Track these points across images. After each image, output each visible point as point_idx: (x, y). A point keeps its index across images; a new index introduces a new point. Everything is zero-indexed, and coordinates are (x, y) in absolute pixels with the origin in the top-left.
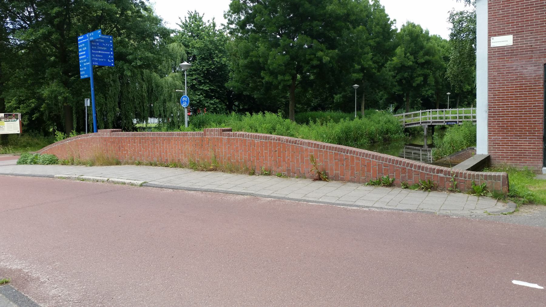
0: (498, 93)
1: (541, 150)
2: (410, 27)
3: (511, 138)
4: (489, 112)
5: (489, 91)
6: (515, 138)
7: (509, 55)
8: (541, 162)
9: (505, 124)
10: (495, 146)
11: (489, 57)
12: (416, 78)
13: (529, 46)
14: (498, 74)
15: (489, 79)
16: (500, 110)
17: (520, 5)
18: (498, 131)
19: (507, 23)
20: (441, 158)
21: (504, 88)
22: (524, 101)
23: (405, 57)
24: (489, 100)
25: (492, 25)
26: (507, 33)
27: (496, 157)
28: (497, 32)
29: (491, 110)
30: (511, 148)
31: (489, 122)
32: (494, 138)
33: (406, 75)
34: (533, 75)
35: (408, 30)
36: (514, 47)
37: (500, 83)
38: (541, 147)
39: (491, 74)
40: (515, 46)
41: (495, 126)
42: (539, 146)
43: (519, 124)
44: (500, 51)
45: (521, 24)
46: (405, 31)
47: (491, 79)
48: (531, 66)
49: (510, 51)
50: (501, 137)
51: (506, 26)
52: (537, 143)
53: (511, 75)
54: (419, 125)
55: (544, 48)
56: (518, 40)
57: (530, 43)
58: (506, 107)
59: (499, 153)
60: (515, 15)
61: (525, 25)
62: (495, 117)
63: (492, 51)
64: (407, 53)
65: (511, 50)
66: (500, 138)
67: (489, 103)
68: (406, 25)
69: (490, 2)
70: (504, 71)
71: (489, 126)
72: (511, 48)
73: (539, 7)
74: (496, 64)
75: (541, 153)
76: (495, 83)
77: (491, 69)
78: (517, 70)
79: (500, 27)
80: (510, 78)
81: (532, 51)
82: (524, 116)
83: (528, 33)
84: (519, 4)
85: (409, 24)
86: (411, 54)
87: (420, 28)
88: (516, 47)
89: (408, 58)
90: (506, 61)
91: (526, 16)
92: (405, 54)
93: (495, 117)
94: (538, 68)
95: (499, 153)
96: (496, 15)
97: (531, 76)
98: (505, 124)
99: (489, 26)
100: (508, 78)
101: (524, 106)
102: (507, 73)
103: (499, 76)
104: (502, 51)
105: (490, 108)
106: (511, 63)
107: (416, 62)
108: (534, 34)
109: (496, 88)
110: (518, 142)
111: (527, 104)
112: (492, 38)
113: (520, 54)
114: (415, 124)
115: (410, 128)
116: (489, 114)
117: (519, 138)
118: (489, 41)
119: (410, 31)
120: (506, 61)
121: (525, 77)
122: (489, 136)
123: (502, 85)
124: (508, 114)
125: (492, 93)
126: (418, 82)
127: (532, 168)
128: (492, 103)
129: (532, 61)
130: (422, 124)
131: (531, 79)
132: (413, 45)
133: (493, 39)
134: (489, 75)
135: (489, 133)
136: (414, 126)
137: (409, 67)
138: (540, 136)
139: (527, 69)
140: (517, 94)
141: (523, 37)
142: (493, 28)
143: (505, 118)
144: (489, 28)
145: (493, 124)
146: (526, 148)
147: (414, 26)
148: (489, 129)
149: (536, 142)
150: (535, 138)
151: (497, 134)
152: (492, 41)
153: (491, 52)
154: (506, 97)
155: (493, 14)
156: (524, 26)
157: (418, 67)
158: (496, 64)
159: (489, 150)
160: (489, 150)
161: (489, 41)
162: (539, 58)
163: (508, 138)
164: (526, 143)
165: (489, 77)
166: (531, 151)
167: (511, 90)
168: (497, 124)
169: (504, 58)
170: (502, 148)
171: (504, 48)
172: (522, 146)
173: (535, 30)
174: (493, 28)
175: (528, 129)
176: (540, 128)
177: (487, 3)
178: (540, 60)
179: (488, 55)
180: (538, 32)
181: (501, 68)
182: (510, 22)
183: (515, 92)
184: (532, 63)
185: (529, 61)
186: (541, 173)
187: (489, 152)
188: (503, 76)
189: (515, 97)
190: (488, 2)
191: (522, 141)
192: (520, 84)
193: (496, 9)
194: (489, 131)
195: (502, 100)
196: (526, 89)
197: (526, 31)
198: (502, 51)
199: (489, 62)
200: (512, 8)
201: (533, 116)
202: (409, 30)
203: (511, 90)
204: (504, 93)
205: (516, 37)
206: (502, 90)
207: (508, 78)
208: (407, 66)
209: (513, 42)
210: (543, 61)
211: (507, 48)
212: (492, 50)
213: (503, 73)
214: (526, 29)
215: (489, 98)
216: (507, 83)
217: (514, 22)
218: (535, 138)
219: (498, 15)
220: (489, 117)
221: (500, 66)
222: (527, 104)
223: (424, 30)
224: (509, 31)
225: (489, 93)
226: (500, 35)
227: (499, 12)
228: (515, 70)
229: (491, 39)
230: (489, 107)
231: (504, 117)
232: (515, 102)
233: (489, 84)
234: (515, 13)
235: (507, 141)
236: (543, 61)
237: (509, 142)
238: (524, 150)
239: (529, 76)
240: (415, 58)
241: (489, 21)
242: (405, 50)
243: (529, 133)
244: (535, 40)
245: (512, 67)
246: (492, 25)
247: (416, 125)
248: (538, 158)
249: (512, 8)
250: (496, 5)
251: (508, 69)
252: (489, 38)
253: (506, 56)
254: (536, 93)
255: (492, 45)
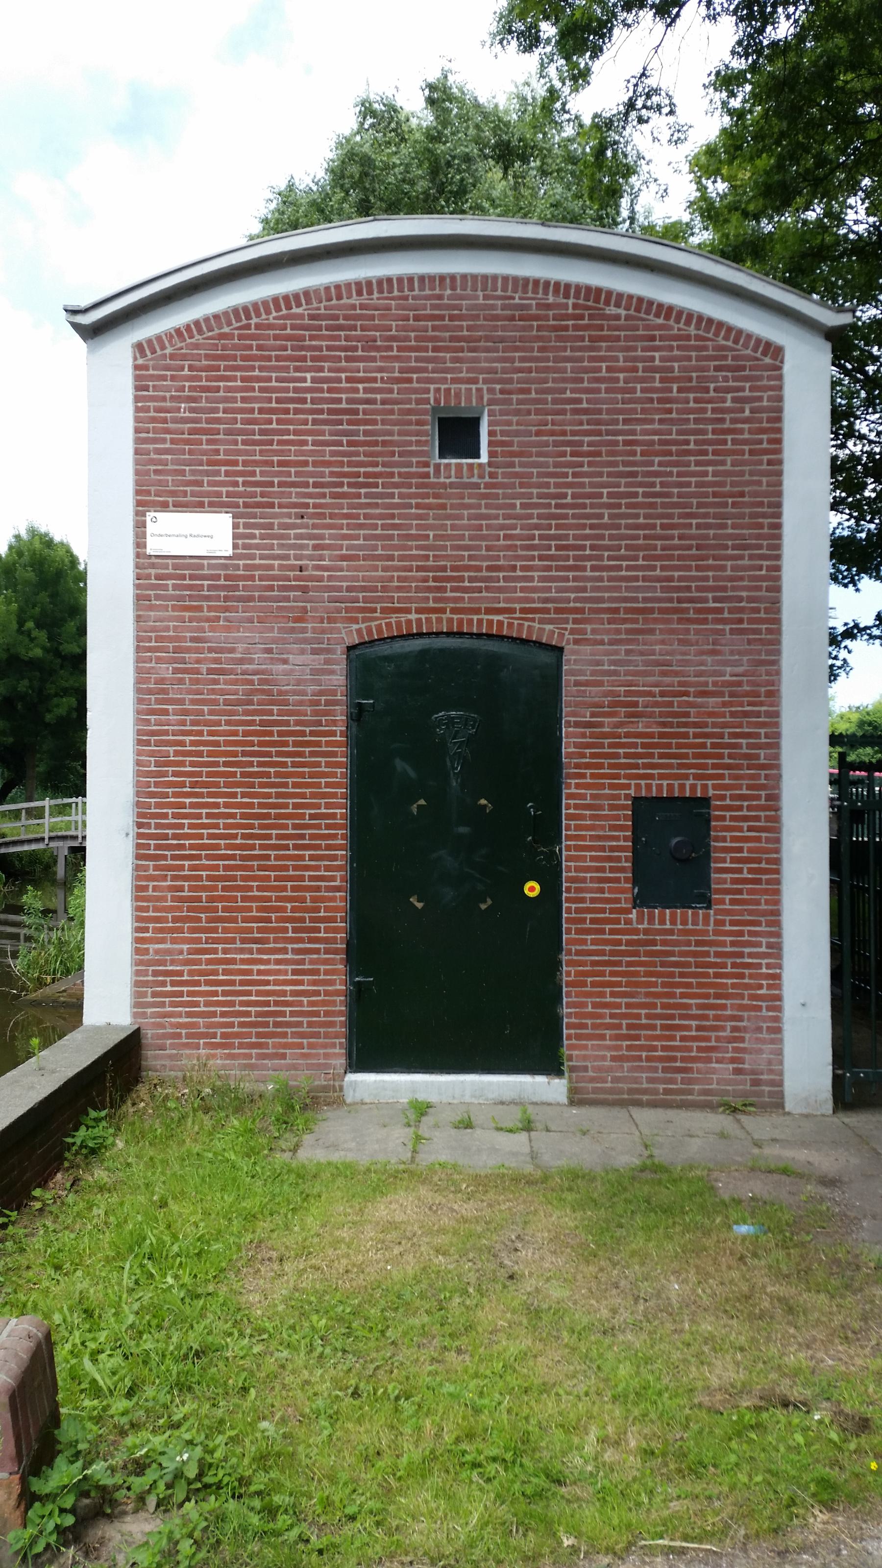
0: (177, 753)
1: (338, 999)
2: (37, 545)
3: (225, 951)
4: (139, 836)
5: (139, 742)
6: (242, 951)
7: (218, 598)
8: (337, 1051)
9: (204, 888)
10: (164, 983)
11: (138, 598)
12: (56, 700)
13: (291, 568)
14: (176, 671)
15: (138, 691)
16: (181, 826)
17: (257, 394)
18: (175, 920)
19: (210, 463)
20: (53, 980)
21: (201, 733)
22: (279, 795)
23: (20, 631)
24: (138, 784)
25: (152, 462)
26: (211, 505)
27: (165, 1036)
28: (173, 493)
29: (148, 826)
30: (225, 994)
31: (138, 878)
32: (157, 952)
33: (23, 685)
34: (311, 688)
35: (29, 550)
36: (237, 567)
37: (185, 712)
38: (338, 987)
39: (149, 671)
40: (241, 562)
41: (164, 899)
42: (332, 983)
43: (259, 889)
44: (183, 577)
45: (262, 473)
46: (20, 554)
47: (150, 692)
48: (303, 652)
49: (222, 582)
50: (185, 947)
51: (207, 473)
52: (326, 972)
53: (226, 682)
54: (41, 846)
55: (345, 584)
56: (253, 536)
57: (297, 558)
58: (208, 816)
59: (180, 1015)
60: (241, 432)
61: (276, 480)
62: (164, 857)
63: (153, 572)
64: (25, 621)
65: (227, 578)
66: (181, 952)
67: (138, 794)
68: (24, 534)
69: (140, 361)
70: (198, 661)
71: (137, 899)
72: (225, 567)
73: (325, 416)
74: (167, 629)
75: (340, 1013)
76: (166, 712)
77: (150, 649)
78: (251, 661)
79: (182, 473)
80: (223, 692)
81: (305, 590)
82: (277, 858)
83: (289, 516)
84: (253, 389)
85: (33, 532)
86: (39, 626)
87: (69, 551)
88: (247, 567)
89: (29, 635)
90: (208, 620)
91: (280, 443)
92: (21, 623)
93: (164, 857)
94: (327, 662)
95: (180, 1015)
96: (165, 421)
97: (303, 693)
98: (204, 888)
99: (137, 463)
100: (213, 692)
101: (278, 816)
102: (210, 671)
103: (181, 681)
104: (192, 577)
105: (142, 818)
106: (228, 629)
107: (57, 653)
108: (311, 522)
109: (166, 733)
110: (255, 968)
111: (286, 806)
112: (152, 514)
113: (261, 599)
114: (30, 841)
115: (18, 855)
116: (138, 846)
117: (260, 951)
118: (140, 526)
119: (35, 554)
120: (208, 620)
121: (280, 693)
122: (138, 940)
123: (194, 724)
124: (217, 847)
125: (152, 754)
126: (62, 711)
127: (303, 1080)
128: (152, 795)
129: (304, 630)
130: (53, 844)
131: (301, 703)
132: (44, 597)
133: (155, 520)
134: (140, 680)
135: (138, 930)
136: (26, 848)
137: (32, 664)
138: (334, 940)
139: (285, 662)
140: (251, 764)
141: (270, 526)
142: (156, 472)
143: (204, 862)
144: (137, 473)
145: (155, 889)
146: (284, 993)
147: (48, 543)
148: (138, 909)
149: (322, 967)
150: (317, 951)
151: (172, 930)
152: (150, 528)
153: (148, 577)
154: (209, 774)
155: (152, 414)
156: (271, 484)
157: (62, 667)
158: (167, 629)
159: (137, 1005)
160: (138, 1004)
161: (140, 526)
162: (330, 620)
163: (215, 952)
164: (285, 972)
165: (138, 681)
166: (301, 1004)
167: (227, 743)
168: (171, 889)
169: (199, 609)
170: (190, 994)
171: (201, 567)
172: (267, 983)
173: (315, 506)
174: (156, 472)
175: (293, 910)
176: (336, 909)
177: (129, 363)
178: (331, 631)
179: (137, 587)
180: (322, 516)
181: (188, 650)
182: (221, 457)
183: (244, 753)
184: (305, 641)
185: (292, 630)
186: (339, 1102)
187: (135, 1015)
188: (197, 681)
189: (243, 774)
190: (135, 359)
191: (268, 962)
192: (262, 723)
193: (168, 395)
194: (138, 919)
195: (194, 785)
196: (285, 744)
197: (281, 506)
198: (192, 577)
199: (138, 619)
200: (226, 400)
201: (312, 858)
202: (34, 553)
203: (227, 743)
204: (200, 754)
205: (246, 526)
206: (193, 743)
207: (213, 692)
208: (26, 659)
209: (235, 546)
210: (344, 635)
211: (210, 566)
212: (153, 566)
213: (197, 672)
214: (281, 495)
215: (139, 774)
216: (211, 713)
217: (593, 984)
218: (317, 951)
219: (175, 421)
220: (138, 857)
221: (184, 639)
222: (286, 806)
223: (81, 560)
224: (219, 494)
225: (139, 753)
226: (181, 506)
227: (178, 410)
228: (241, 661)
229: (148, 519)
230: (140, 815)
231: (198, 857)
232: (244, 795)
233: (138, 712)
234: (239, 426)
235: (209, 962)
236: (344, 635)
237: (221, 967)
238: (277, 1003)
239: (295, 693)
240: (50, 638)
241: (138, 441)
242: (21, 610)
243: (295, 930)
244: (316, 547)
245: (232, 650)
246: (152, 462)
247: (34, 847)
248: (327, 1035)
249: (226, 400)
250: (164, 378)
251: (214, 655)
252: (137, 513)
253: (207, 598)
254: (318, 764)
255: (154, 546)
